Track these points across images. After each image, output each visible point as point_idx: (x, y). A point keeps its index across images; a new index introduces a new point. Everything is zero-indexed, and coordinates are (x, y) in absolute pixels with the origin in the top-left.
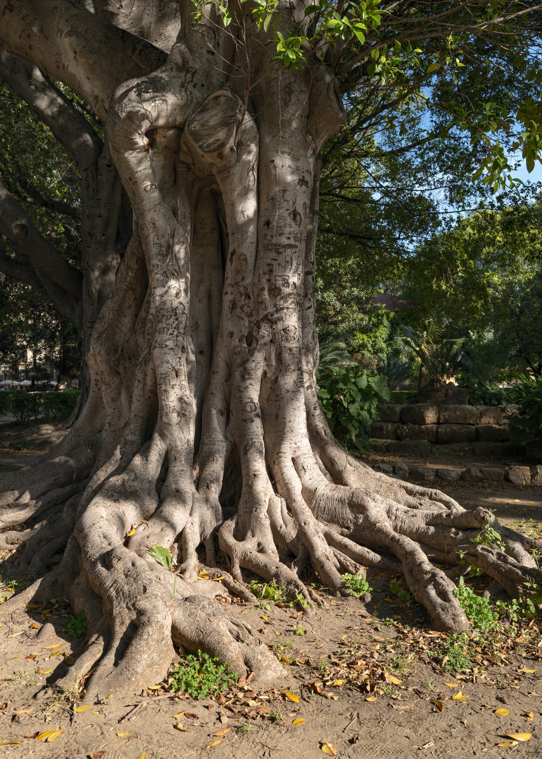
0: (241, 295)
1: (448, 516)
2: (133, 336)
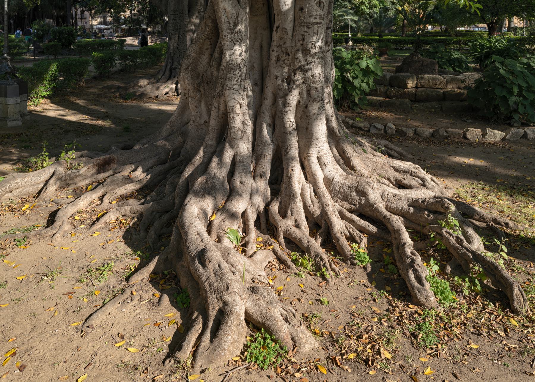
0: (283, 53)
2: (210, 68)
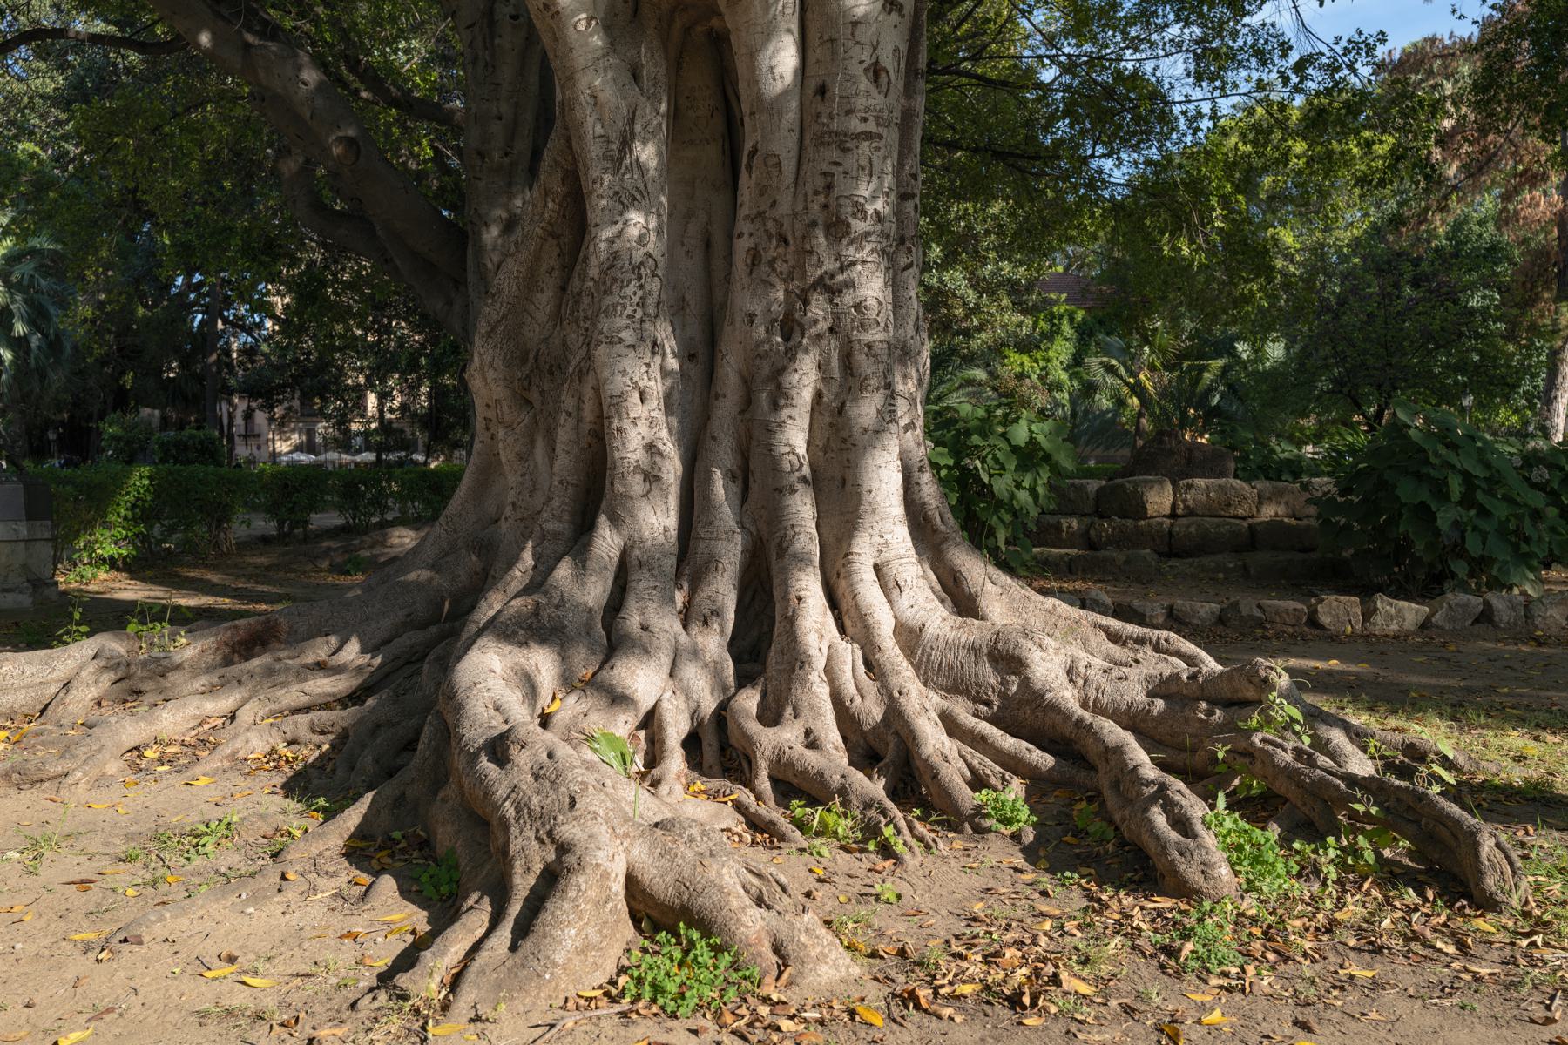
0: (770, 238)
1: (1193, 677)
